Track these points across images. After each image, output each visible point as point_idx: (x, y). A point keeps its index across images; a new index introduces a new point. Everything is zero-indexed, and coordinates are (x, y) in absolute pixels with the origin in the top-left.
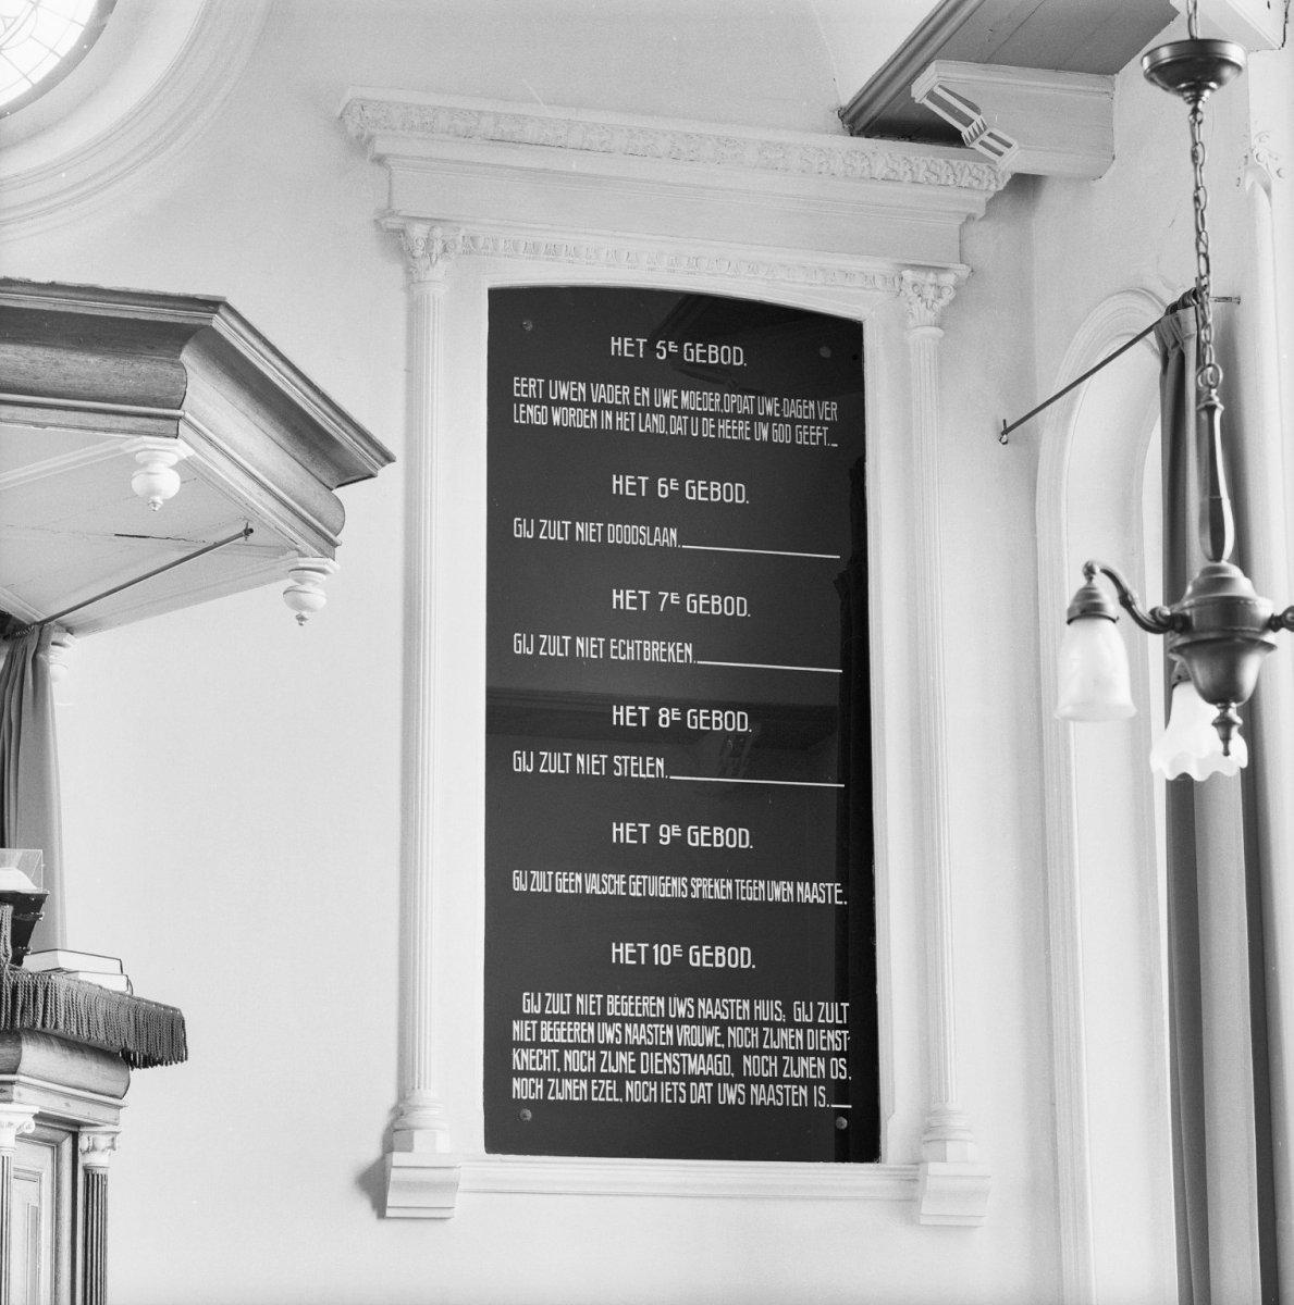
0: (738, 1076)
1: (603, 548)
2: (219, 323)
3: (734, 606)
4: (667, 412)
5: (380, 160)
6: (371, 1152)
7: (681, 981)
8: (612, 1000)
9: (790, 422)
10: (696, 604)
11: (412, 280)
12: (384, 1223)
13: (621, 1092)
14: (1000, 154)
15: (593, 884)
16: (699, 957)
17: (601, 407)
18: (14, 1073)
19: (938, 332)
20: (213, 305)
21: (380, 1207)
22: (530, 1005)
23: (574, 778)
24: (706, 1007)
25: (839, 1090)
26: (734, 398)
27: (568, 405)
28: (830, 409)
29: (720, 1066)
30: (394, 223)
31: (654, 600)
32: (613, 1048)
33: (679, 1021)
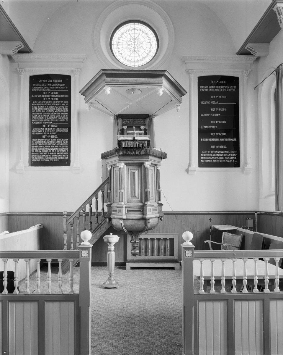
0: (225, 159)
1: (210, 104)
2: (166, 73)
3: (224, 109)
4: (217, 89)
5: (186, 63)
6: (187, 168)
7: (219, 149)
8: (211, 152)
9: (231, 89)
10: (220, 109)
11: (189, 77)
12: (188, 175)
13: (212, 161)
14: (255, 54)
15: (209, 140)
16: (221, 147)
17: (210, 89)
18: (149, 159)
19: (247, 77)
20: (165, 71)
21: (188, 173)
22: (203, 152)
23: (207, 116)
24: (221, 152)
25: (235, 160)
26: (224, 87)
27: (206, 89)
28: (235, 87)
29: (223, 158)
30: (187, 70)
31: (216, 109)
32: (212, 156)
33: (218, 154)
